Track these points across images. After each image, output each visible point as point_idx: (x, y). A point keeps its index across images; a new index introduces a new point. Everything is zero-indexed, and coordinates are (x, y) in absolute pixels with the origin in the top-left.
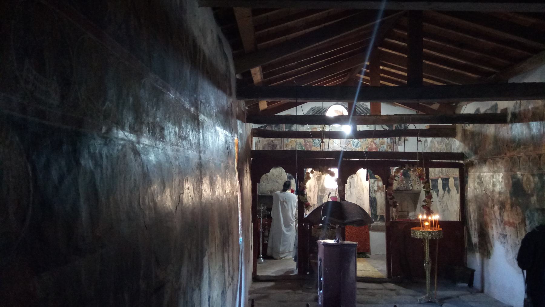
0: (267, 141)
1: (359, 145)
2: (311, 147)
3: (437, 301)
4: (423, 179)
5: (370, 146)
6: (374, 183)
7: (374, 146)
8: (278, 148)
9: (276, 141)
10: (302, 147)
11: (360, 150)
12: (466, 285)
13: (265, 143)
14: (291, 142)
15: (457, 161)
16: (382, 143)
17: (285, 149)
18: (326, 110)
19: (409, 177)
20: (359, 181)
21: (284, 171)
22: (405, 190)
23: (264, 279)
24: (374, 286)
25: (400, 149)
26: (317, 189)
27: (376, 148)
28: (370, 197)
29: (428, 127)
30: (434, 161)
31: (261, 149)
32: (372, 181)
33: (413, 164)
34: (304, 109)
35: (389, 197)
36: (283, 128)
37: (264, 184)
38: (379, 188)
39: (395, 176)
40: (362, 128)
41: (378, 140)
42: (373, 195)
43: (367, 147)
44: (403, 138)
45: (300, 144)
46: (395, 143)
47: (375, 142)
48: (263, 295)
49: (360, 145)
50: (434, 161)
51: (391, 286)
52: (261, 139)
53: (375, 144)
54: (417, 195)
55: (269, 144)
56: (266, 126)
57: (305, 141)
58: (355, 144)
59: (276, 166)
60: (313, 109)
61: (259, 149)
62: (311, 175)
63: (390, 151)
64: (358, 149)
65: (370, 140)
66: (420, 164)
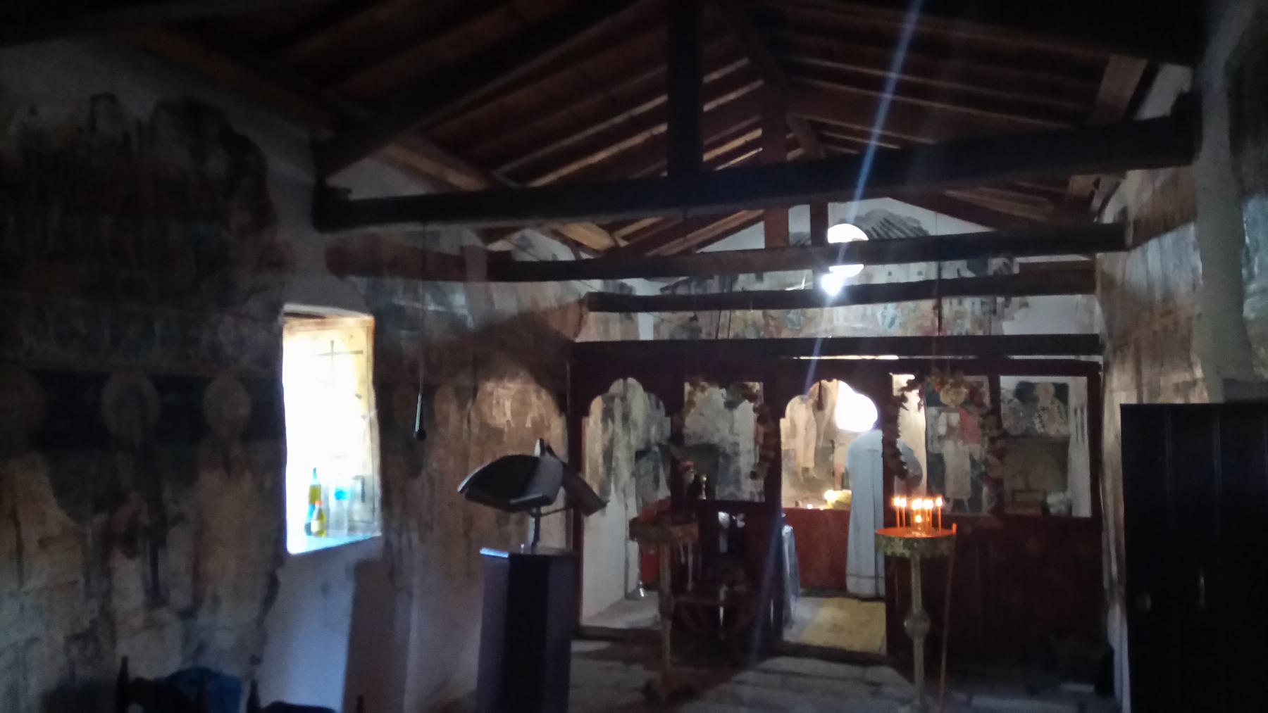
1: (897, 322)
2: (779, 330)
6: (936, 418)
10: (758, 333)
11: (598, 339)
12: (1088, 689)
15: (1083, 358)
19: (1036, 400)
22: (1024, 436)
25: (1009, 328)
26: (813, 432)
28: (927, 452)
30: (971, 357)
32: (933, 410)
33: (955, 367)
38: (950, 429)
42: (936, 448)
44: (1016, 300)
45: (754, 324)
46: (994, 312)
49: (883, 319)
50: (895, 357)
52: (666, 315)
54: (1060, 448)
57: (765, 316)
58: (888, 320)
63: (980, 333)
64: (895, 332)
66: (970, 368)
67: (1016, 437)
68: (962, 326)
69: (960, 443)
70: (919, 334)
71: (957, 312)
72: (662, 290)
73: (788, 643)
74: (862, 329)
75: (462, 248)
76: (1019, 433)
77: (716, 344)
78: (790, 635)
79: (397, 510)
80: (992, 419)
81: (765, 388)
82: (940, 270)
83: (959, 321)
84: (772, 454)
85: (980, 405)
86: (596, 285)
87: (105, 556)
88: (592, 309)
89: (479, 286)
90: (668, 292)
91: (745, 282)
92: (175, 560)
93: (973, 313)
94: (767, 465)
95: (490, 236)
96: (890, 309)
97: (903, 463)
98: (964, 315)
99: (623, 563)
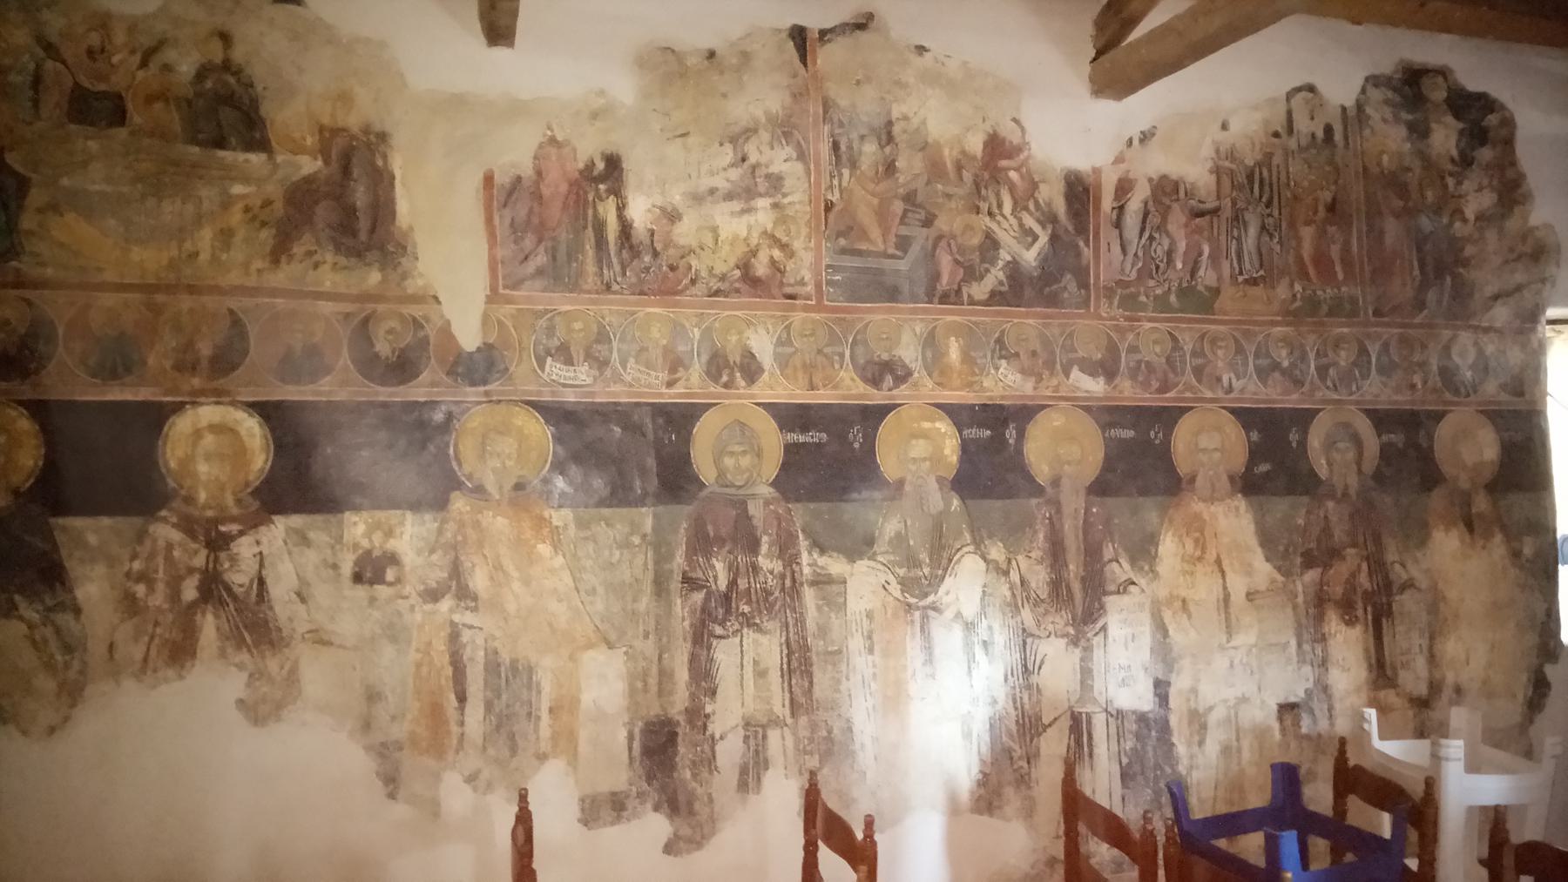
40: (837, 366)
87: (1320, 618)
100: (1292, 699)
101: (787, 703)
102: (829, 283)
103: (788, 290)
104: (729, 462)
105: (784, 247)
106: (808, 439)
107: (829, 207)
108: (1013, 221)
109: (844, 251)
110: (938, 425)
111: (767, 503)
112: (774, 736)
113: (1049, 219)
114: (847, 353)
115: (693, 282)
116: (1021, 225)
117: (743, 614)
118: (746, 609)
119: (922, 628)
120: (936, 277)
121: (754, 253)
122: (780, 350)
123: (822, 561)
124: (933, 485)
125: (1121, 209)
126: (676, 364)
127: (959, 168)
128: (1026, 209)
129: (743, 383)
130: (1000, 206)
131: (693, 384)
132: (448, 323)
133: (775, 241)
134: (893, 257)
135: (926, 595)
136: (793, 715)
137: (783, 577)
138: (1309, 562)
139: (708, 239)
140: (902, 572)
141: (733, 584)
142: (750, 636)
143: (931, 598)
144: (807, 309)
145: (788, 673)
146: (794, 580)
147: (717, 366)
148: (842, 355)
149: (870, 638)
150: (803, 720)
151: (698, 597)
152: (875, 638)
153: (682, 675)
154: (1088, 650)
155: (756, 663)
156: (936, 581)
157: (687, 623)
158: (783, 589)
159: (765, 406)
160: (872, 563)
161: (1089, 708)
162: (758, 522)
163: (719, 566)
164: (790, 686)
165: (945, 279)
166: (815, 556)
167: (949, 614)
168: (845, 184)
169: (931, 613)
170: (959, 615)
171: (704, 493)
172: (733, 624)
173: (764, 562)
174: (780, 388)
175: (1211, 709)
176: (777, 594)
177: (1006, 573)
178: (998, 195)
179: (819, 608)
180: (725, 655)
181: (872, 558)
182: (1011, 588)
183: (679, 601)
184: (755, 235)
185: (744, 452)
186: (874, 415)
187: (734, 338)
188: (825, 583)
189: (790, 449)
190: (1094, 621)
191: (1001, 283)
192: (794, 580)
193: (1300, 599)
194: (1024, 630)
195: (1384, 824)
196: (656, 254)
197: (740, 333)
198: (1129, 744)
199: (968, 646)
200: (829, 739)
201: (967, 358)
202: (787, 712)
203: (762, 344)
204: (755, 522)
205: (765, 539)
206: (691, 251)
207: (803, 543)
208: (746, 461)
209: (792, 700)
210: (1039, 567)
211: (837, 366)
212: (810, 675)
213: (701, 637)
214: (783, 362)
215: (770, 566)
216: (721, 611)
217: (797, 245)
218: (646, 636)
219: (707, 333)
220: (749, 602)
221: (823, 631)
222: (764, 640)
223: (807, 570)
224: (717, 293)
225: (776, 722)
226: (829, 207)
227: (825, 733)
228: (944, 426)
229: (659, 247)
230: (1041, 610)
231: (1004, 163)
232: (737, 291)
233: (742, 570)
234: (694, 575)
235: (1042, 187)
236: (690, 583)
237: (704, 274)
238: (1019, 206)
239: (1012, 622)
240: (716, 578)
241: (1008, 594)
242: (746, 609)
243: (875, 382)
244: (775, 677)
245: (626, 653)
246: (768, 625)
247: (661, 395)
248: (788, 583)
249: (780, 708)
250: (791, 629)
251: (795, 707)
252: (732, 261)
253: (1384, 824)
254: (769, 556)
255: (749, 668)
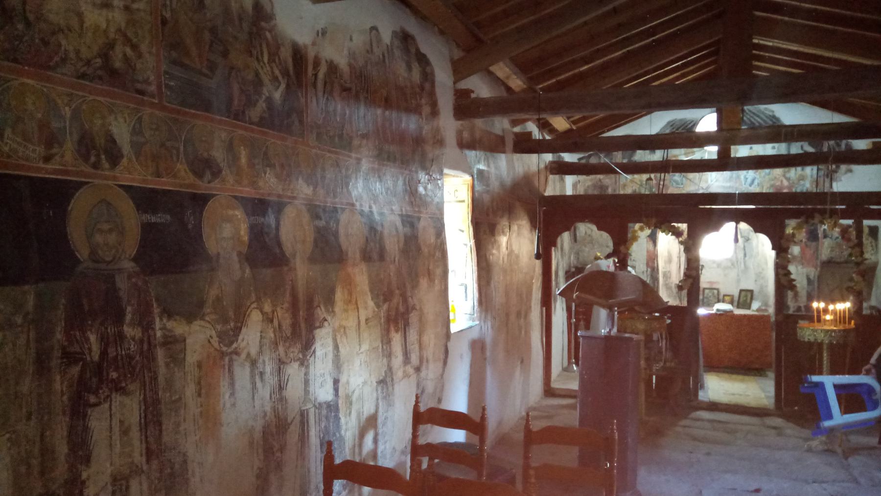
0: (591, 180)
1: (756, 182)
3: (839, 450)
4: (849, 240)
5: (778, 183)
7: (786, 183)
8: (610, 191)
9: (606, 179)
13: (589, 183)
14: (632, 181)
16: (802, 178)
17: (622, 192)
18: (695, 124)
20: (760, 245)
21: (594, 228)
23: (563, 393)
24: (745, 419)
27: (790, 187)
29: (870, 147)
31: (582, 193)
34: (654, 124)
35: (781, 272)
36: (619, 157)
37: (587, 249)
39: (793, 235)
40: (175, 159)
41: (794, 173)
43: (772, 186)
44: (843, 167)
47: (788, 175)
48: (544, 414)
50: (753, 207)
51: (778, 421)
52: (582, 178)
53: (788, 179)
55: (595, 186)
56: (590, 156)
58: (749, 180)
59: (582, 219)
60: (671, 124)
61: (578, 193)
62: (640, 233)
64: (755, 189)
65: (778, 172)
66: (845, 215)
67: (838, 263)
68: (804, 185)
69: (800, 268)
70: (771, 191)
71: (801, 175)
72: (580, 159)
73: (702, 402)
74: (730, 187)
75: (503, 130)
76: (842, 260)
77: (616, 197)
78: (702, 396)
79: (484, 304)
80: (857, 249)
81: (689, 227)
82: (789, 149)
83: (802, 182)
84: (694, 273)
85: (849, 240)
86: (548, 157)
87: (388, 331)
88: (552, 173)
89: (510, 155)
90: (583, 161)
91: (641, 156)
92: (413, 335)
93: (812, 176)
94: (690, 281)
95: (515, 123)
96: (751, 174)
97: (794, 280)
98: (804, 179)
99: (443, 349)
100: (381, 378)
101: (144, 452)
102: (167, 86)
103: (139, 86)
104: (99, 238)
105: (134, 47)
106: (159, 220)
107: (164, 22)
108: (268, 68)
109: (174, 62)
110: (237, 213)
111: (130, 277)
112: (134, 485)
113: (285, 73)
114: (182, 148)
115: (64, 60)
116: (273, 72)
117: (113, 380)
118: (114, 375)
119: (229, 370)
120: (230, 100)
121: (111, 45)
122: (135, 139)
123: (170, 324)
124: (235, 258)
125: (316, 75)
126: (51, 140)
127: (241, 19)
128: (274, 61)
129: (107, 166)
130: (262, 54)
131: (66, 161)
132: (443, 203)
133: (128, 41)
134: (205, 75)
135: (232, 343)
136: (148, 461)
137: (142, 341)
138: (385, 301)
139: (75, 23)
140: (219, 327)
141: (104, 353)
142: (117, 398)
143: (235, 345)
144: (152, 105)
145: (144, 427)
146: (149, 343)
147: (87, 146)
148: (178, 150)
149: (199, 383)
150: (155, 464)
151: (75, 370)
152: (203, 383)
153: (62, 449)
154: (307, 367)
155: (121, 422)
156: (238, 330)
157: (65, 398)
158: (141, 353)
159: (127, 189)
160: (202, 323)
161: (309, 406)
162: (123, 294)
163: (93, 338)
164: (146, 437)
165: (236, 102)
166: (165, 320)
167: (243, 356)
168: (174, 6)
169: (234, 357)
170: (248, 354)
171: (80, 268)
172: (104, 392)
173: (128, 331)
174: (134, 173)
175: (353, 392)
176: (138, 358)
177: (272, 321)
178: (261, 46)
179: (167, 365)
180: (98, 423)
181: (202, 319)
182: (274, 332)
183: (58, 378)
184: (112, 30)
185: (110, 231)
186: (201, 200)
187: (99, 122)
188: (171, 343)
189: (147, 228)
190: (310, 348)
191: (264, 111)
192: (149, 343)
193: (382, 320)
194: (280, 360)
195: (458, 436)
196: (28, 24)
197: (103, 118)
198: (323, 425)
199: (252, 376)
200: (172, 475)
201: (251, 165)
202: (144, 459)
203: (121, 130)
204: (121, 293)
205: (129, 309)
206: (61, 30)
207: (156, 310)
208: (112, 238)
209: (147, 449)
210: (287, 315)
211: (175, 159)
212: (160, 424)
213: (78, 409)
214: (137, 148)
215: (133, 334)
216: (94, 380)
217: (144, 48)
218: (29, 418)
219: (76, 114)
220: (116, 369)
221: (170, 383)
222: (127, 400)
223: (159, 334)
224: (83, 76)
225: (137, 471)
226: (164, 22)
227: (169, 470)
228: (239, 214)
229: (31, 17)
230: (287, 344)
231: (263, 24)
232: (100, 78)
233: (111, 339)
234: (72, 350)
235: (282, 49)
236: (69, 358)
237: (72, 55)
238: (271, 60)
239: (274, 355)
240: (90, 349)
241: (272, 335)
242: (114, 375)
243: (199, 175)
244: (135, 434)
245: (9, 439)
246: (131, 387)
247: (39, 170)
248: (145, 347)
249: (139, 458)
250: (147, 388)
251: (149, 454)
252: (96, 49)
253: (458, 436)
254: (132, 324)
255: (116, 429)
